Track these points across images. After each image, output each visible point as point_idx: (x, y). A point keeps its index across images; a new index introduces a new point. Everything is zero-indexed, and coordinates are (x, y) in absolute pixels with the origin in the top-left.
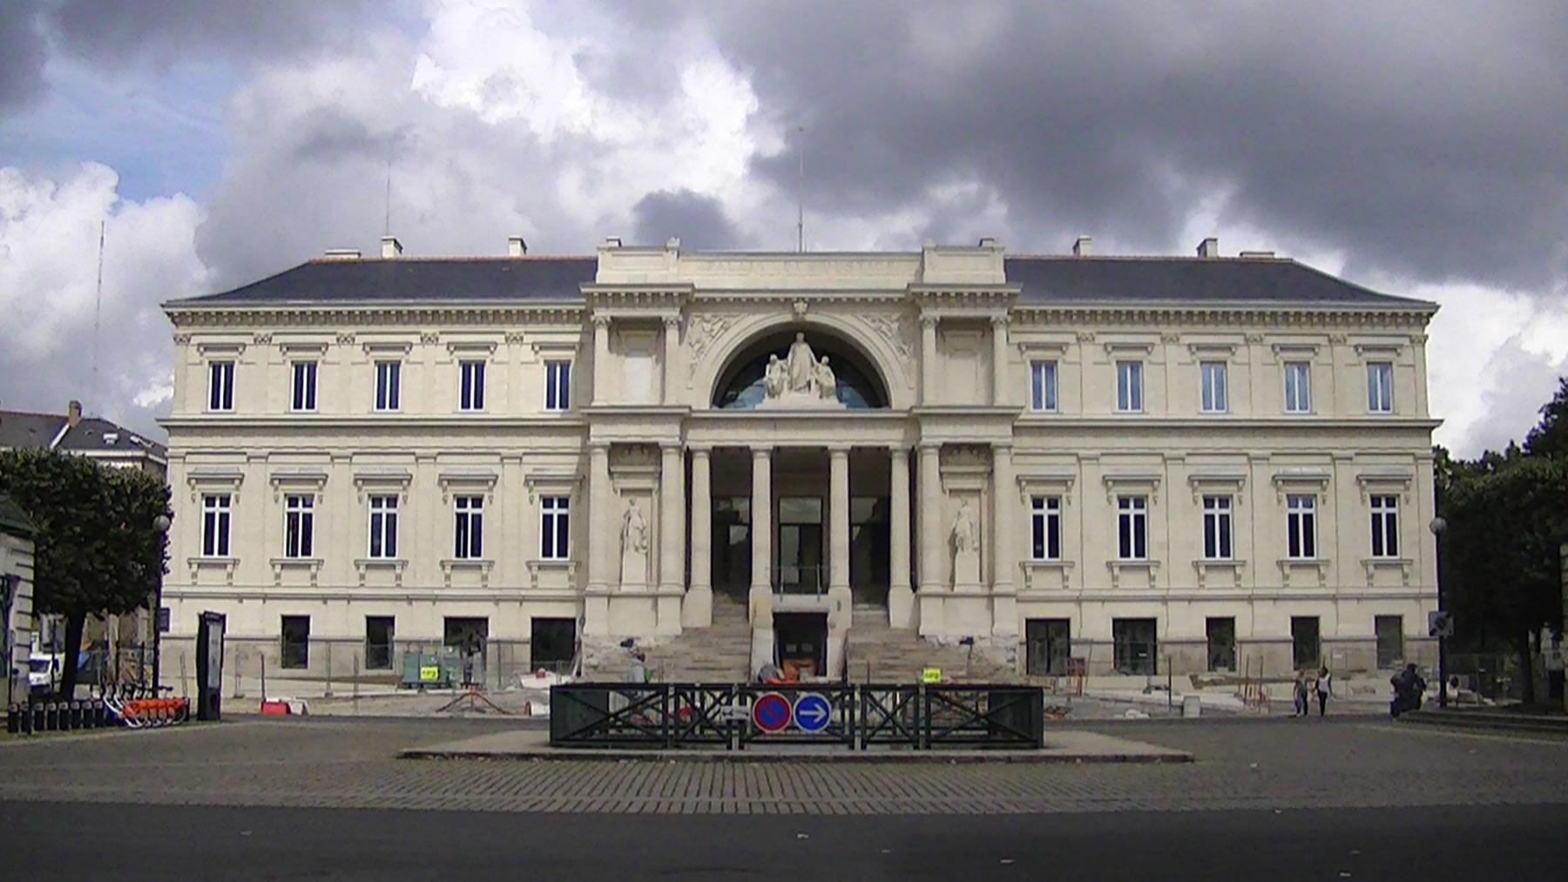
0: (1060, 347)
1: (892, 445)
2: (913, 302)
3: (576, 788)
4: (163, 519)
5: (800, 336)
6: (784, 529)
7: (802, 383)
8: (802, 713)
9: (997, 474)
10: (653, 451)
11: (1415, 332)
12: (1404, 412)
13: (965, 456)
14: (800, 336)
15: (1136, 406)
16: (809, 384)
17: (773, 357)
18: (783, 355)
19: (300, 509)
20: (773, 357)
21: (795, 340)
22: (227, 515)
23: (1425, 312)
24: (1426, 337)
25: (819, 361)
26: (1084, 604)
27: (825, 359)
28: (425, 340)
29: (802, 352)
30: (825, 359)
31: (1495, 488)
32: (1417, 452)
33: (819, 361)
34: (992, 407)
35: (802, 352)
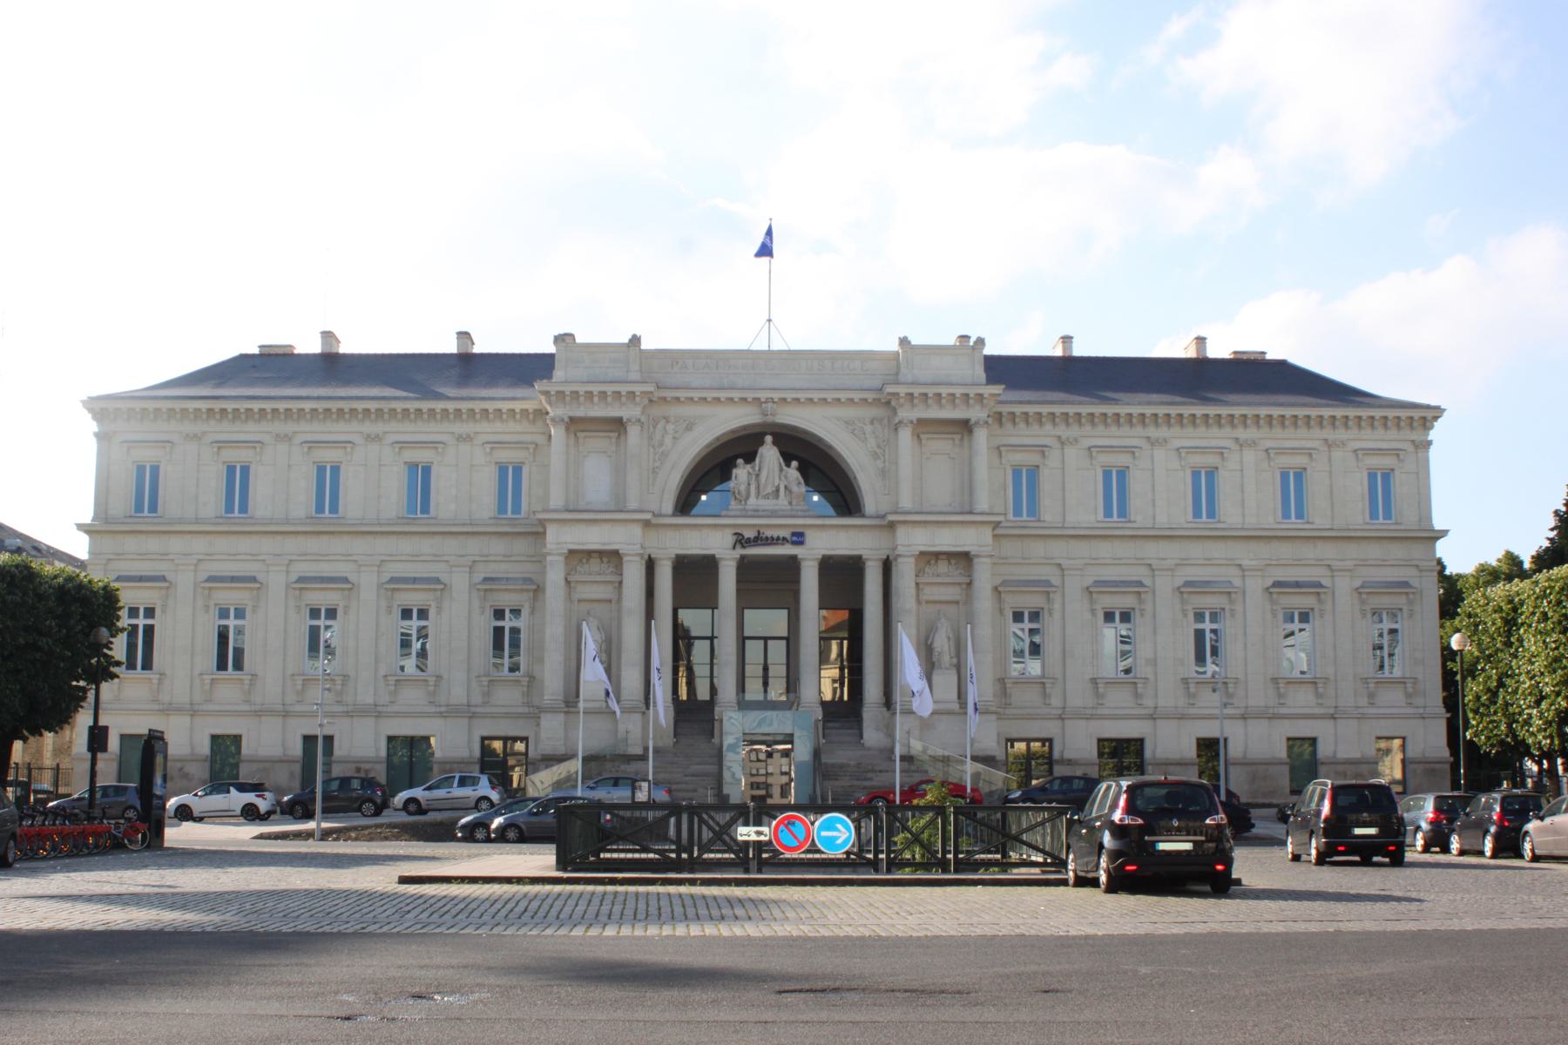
0: (1131, 450)
1: (865, 554)
2: (888, 403)
3: (454, 912)
4: (104, 631)
5: (769, 439)
6: (748, 642)
7: (770, 489)
8: (824, 833)
9: (976, 584)
10: (613, 557)
11: (1415, 436)
12: (1409, 520)
13: (595, 562)
14: (769, 439)
15: (1300, 516)
16: (778, 490)
17: (740, 461)
18: (750, 458)
19: (507, 623)
20: (740, 461)
21: (762, 443)
22: (152, 627)
23: (1429, 414)
24: (1430, 443)
25: (788, 465)
26: (1250, 722)
27: (794, 464)
28: (280, 438)
29: (769, 453)
30: (794, 464)
31: (17, 566)
32: (1420, 563)
33: (788, 465)
34: (971, 513)
35: (769, 453)
